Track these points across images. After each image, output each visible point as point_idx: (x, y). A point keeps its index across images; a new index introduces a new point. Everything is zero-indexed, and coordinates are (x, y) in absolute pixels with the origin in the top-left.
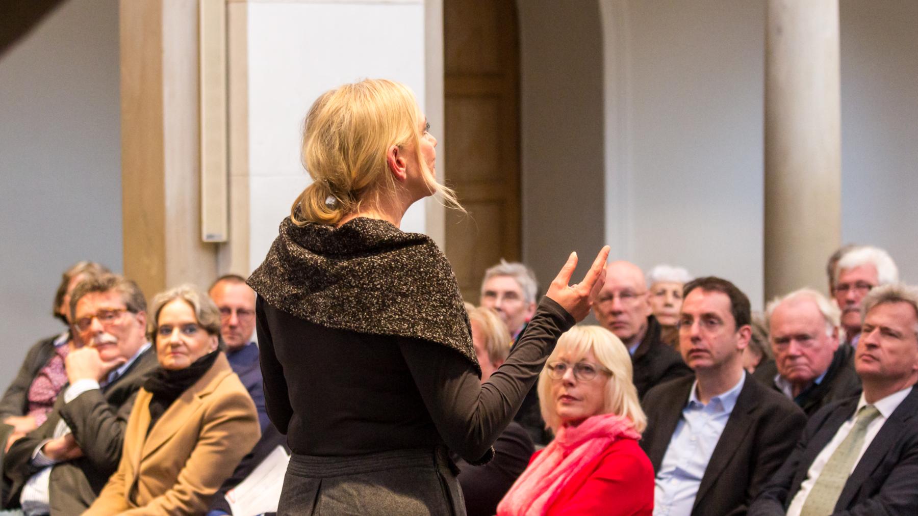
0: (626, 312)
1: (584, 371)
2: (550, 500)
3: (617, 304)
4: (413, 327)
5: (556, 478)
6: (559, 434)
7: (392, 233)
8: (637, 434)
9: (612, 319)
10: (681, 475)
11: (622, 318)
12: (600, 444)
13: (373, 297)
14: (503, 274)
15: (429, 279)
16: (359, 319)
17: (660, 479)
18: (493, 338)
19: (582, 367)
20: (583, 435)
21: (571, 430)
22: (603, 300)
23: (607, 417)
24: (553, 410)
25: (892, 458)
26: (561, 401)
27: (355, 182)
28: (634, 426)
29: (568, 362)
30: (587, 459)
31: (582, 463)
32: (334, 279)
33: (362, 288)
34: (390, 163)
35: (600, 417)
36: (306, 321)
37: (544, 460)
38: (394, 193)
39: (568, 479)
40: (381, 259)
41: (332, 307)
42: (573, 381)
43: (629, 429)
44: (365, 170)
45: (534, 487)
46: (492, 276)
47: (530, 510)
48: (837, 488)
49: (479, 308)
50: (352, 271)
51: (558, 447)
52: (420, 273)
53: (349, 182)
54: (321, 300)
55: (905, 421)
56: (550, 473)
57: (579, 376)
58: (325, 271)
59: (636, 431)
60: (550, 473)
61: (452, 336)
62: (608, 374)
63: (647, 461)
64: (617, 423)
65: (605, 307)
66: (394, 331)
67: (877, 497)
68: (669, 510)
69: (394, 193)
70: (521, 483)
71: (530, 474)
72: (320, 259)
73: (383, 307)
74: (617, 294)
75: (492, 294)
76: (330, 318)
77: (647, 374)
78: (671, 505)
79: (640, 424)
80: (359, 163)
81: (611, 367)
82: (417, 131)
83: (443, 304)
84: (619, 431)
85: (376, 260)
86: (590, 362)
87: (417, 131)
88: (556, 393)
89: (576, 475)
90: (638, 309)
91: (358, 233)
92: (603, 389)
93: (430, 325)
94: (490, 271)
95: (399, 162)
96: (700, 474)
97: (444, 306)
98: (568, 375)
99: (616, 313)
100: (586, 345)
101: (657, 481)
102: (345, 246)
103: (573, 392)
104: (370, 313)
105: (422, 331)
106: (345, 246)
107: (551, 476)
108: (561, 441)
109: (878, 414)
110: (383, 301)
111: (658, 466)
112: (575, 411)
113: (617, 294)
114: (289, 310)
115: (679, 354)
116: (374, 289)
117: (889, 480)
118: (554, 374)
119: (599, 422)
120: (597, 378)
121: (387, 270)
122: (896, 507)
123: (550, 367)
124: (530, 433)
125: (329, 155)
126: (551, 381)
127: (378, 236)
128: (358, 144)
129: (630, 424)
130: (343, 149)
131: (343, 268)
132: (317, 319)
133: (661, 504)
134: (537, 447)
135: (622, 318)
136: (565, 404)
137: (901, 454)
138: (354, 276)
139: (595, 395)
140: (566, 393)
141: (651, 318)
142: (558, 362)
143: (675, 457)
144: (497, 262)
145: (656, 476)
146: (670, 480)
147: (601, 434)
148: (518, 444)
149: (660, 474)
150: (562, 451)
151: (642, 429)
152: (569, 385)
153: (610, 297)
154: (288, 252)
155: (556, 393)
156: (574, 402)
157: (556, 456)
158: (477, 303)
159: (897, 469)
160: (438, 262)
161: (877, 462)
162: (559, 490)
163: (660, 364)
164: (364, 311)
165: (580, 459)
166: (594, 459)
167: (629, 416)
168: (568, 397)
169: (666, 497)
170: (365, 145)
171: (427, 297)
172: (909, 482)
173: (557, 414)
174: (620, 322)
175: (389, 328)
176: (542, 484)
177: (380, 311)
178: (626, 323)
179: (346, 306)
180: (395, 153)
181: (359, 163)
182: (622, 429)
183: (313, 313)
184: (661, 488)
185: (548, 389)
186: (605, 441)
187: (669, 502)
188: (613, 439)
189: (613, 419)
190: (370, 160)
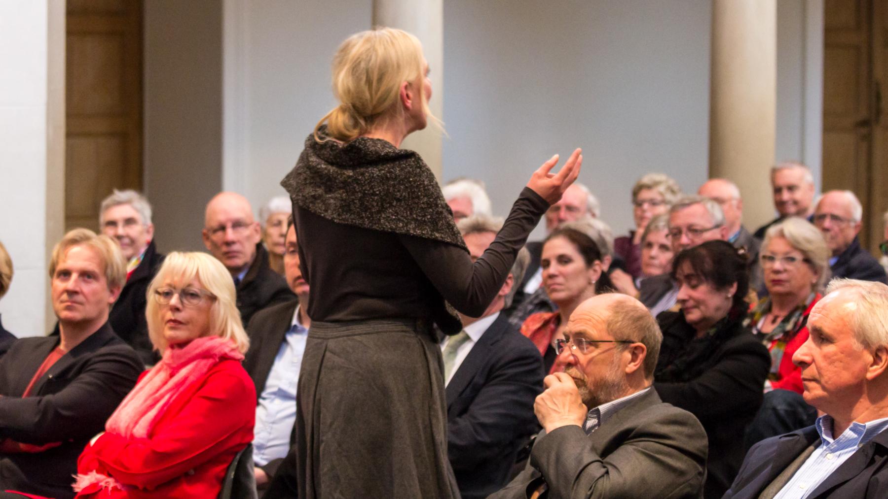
0: (239, 242)
1: (189, 297)
2: (156, 417)
3: (231, 234)
4: (407, 226)
5: (162, 396)
6: (167, 354)
7: (387, 150)
8: (240, 355)
9: (225, 249)
10: (282, 395)
11: (236, 247)
12: (205, 365)
13: (373, 200)
14: (119, 203)
15: (417, 187)
16: (362, 217)
17: (264, 399)
18: (112, 266)
19: (187, 293)
20: (189, 356)
21: (178, 352)
22: (215, 231)
23: (212, 339)
24: (160, 333)
25: (479, 380)
26: (169, 325)
27: (375, 107)
28: (238, 347)
29: (175, 288)
30: (192, 378)
31: (188, 382)
32: (341, 185)
33: (364, 194)
34: (402, 96)
35: (205, 339)
36: (320, 216)
37: (151, 379)
38: (401, 119)
39: (174, 397)
40: (380, 171)
41: (340, 207)
42: (180, 306)
43: (233, 350)
44: (382, 100)
45: (142, 405)
46: (108, 207)
47: (137, 426)
48: (258, 433)
49: (100, 236)
50: (356, 180)
51: (165, 367)
52: (410, 182)
53: (370, 107)
54: (332, 201)
55: (492, 345)
56: (158, 390)
57: (185, 301)
58: (336, 178)
59: (240, 352)
60: (158, 390)
61: (437, 231)
62: (213, 298)
63: (249, 382)
64: (222, 344)
65: (218, 237)
66: (391, 228)
67: (465, 416)
68: (272, 428)
69: (401, 119)
70: (129, 401)
71: (138, 392)
72: (332, 169)
73: (382, 210)
74: (229, 225)
75: (113, 223)
76: (339, 215)
77: (254, 299)
78: (273, 423)
79: (243, 345)
80: (379, 93)
81: (216, 292)
82: (422, 72)
83: (430, 205)
84: (222, 352)
85: (375, 171)
86: (195, 289)
87: (422, 72)
88: (163, 318)
89: (182, 393)
90: (249, 238)
91: (360, 149)
92: (208, 312)
93: (421, 224)
94: (105, 203)
95: (407, 95)
96: (293, 391)
97: (431, 207)
98: (174, 300)
99: (228, 244)
100: (191, 271)
101: (261, 401)
102: (351, 160)
103: (180, 316)
104: (371, 214)
105: (414, 229)
106: (351, 160)
107: (157, 395)
108: (167, 362)
109: (467, 338)
110: (382, 205)
111: (261, 386)
112: (181, 334)
113: (229, 225)
114: (309, 207)
115: (285, 280)
116: (374, 194)
117: (477, 400)
118: (162, 300)
119: (206, 343)
120: (202, 303)
121: (384, 179)
122: (483, 426)
123: (157, 292)
124: (140, 354)
125: (358, 86)
126: (159, 306)
127: (377, 152)
128: (380, 80)
129: (234, 346)
130: (369, 82)
131: (349, 177)
132: (328, 215)
133: (262, 422)
134: (147, 367)
135: (236, 247)
136: (172, 328)
137: (491, 372)
138: (358, 184)
139: (200, 319)
140: (173, 318)
141: (259, 246)
142: (165, 289)
143: (278, 378)
144: (110, 192)
145: (259, 396)
146: (273, 400)
147: (206, 355)
148: (128, 364)
149: (264, 395)
150: (169, 372)
151: (245, 350)
152: (176, 309)
153: (222, 228)
154: (309, 161)
155: (163, 318)
156: (180, 326)
157: (163, 375)
158: (98, 232)
159: (485, 390)
160: (423, 172)
161: (466, 383)
162: (165, 408)
163: (266, 290)
164: (366, 211)
165: (186, 378)
166: (198, 379)
167: (233, 338)
168: (175, 321)
169: (268, 415)
170: (385, 82)
171: (416, 200)
172: (495, 402)
173: (164, 337)
174: (234, 252)
175: (388, 226)
176: (149, 402)
177: (379, 212)
178: (238, 252)
179: (352, 207)
180: (406, 87)
181: (379, 93)
182: (227, 350)
183: (326, 211)
184: (264, 407)
185: (155, 313)
186: (211, 361)
187: (272, 420)
188: (217, 360)
189: (217, 341)
190: (388, 91)
